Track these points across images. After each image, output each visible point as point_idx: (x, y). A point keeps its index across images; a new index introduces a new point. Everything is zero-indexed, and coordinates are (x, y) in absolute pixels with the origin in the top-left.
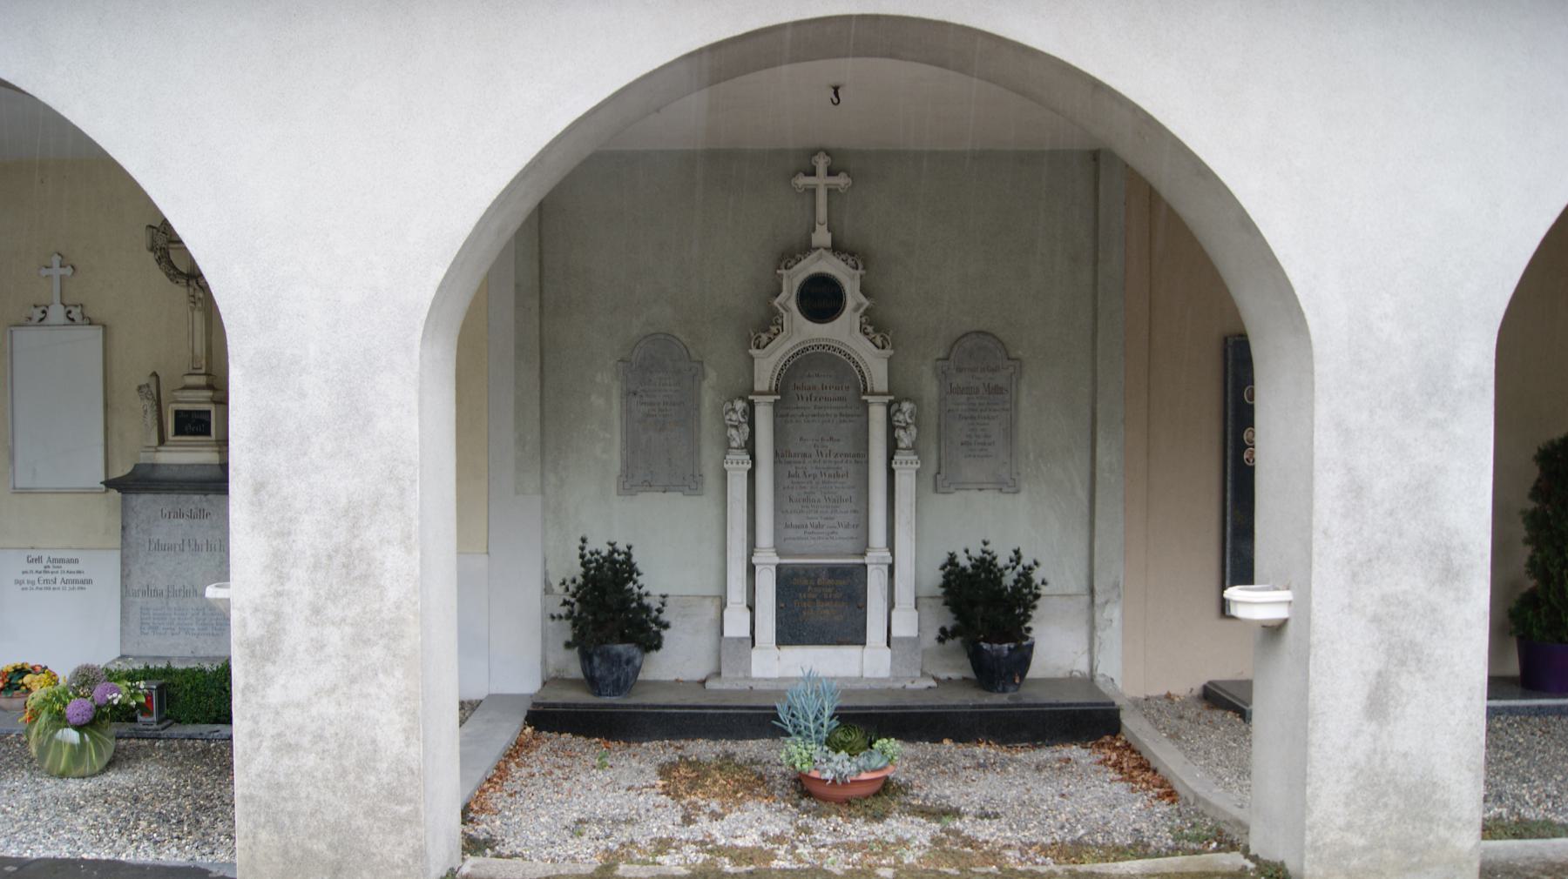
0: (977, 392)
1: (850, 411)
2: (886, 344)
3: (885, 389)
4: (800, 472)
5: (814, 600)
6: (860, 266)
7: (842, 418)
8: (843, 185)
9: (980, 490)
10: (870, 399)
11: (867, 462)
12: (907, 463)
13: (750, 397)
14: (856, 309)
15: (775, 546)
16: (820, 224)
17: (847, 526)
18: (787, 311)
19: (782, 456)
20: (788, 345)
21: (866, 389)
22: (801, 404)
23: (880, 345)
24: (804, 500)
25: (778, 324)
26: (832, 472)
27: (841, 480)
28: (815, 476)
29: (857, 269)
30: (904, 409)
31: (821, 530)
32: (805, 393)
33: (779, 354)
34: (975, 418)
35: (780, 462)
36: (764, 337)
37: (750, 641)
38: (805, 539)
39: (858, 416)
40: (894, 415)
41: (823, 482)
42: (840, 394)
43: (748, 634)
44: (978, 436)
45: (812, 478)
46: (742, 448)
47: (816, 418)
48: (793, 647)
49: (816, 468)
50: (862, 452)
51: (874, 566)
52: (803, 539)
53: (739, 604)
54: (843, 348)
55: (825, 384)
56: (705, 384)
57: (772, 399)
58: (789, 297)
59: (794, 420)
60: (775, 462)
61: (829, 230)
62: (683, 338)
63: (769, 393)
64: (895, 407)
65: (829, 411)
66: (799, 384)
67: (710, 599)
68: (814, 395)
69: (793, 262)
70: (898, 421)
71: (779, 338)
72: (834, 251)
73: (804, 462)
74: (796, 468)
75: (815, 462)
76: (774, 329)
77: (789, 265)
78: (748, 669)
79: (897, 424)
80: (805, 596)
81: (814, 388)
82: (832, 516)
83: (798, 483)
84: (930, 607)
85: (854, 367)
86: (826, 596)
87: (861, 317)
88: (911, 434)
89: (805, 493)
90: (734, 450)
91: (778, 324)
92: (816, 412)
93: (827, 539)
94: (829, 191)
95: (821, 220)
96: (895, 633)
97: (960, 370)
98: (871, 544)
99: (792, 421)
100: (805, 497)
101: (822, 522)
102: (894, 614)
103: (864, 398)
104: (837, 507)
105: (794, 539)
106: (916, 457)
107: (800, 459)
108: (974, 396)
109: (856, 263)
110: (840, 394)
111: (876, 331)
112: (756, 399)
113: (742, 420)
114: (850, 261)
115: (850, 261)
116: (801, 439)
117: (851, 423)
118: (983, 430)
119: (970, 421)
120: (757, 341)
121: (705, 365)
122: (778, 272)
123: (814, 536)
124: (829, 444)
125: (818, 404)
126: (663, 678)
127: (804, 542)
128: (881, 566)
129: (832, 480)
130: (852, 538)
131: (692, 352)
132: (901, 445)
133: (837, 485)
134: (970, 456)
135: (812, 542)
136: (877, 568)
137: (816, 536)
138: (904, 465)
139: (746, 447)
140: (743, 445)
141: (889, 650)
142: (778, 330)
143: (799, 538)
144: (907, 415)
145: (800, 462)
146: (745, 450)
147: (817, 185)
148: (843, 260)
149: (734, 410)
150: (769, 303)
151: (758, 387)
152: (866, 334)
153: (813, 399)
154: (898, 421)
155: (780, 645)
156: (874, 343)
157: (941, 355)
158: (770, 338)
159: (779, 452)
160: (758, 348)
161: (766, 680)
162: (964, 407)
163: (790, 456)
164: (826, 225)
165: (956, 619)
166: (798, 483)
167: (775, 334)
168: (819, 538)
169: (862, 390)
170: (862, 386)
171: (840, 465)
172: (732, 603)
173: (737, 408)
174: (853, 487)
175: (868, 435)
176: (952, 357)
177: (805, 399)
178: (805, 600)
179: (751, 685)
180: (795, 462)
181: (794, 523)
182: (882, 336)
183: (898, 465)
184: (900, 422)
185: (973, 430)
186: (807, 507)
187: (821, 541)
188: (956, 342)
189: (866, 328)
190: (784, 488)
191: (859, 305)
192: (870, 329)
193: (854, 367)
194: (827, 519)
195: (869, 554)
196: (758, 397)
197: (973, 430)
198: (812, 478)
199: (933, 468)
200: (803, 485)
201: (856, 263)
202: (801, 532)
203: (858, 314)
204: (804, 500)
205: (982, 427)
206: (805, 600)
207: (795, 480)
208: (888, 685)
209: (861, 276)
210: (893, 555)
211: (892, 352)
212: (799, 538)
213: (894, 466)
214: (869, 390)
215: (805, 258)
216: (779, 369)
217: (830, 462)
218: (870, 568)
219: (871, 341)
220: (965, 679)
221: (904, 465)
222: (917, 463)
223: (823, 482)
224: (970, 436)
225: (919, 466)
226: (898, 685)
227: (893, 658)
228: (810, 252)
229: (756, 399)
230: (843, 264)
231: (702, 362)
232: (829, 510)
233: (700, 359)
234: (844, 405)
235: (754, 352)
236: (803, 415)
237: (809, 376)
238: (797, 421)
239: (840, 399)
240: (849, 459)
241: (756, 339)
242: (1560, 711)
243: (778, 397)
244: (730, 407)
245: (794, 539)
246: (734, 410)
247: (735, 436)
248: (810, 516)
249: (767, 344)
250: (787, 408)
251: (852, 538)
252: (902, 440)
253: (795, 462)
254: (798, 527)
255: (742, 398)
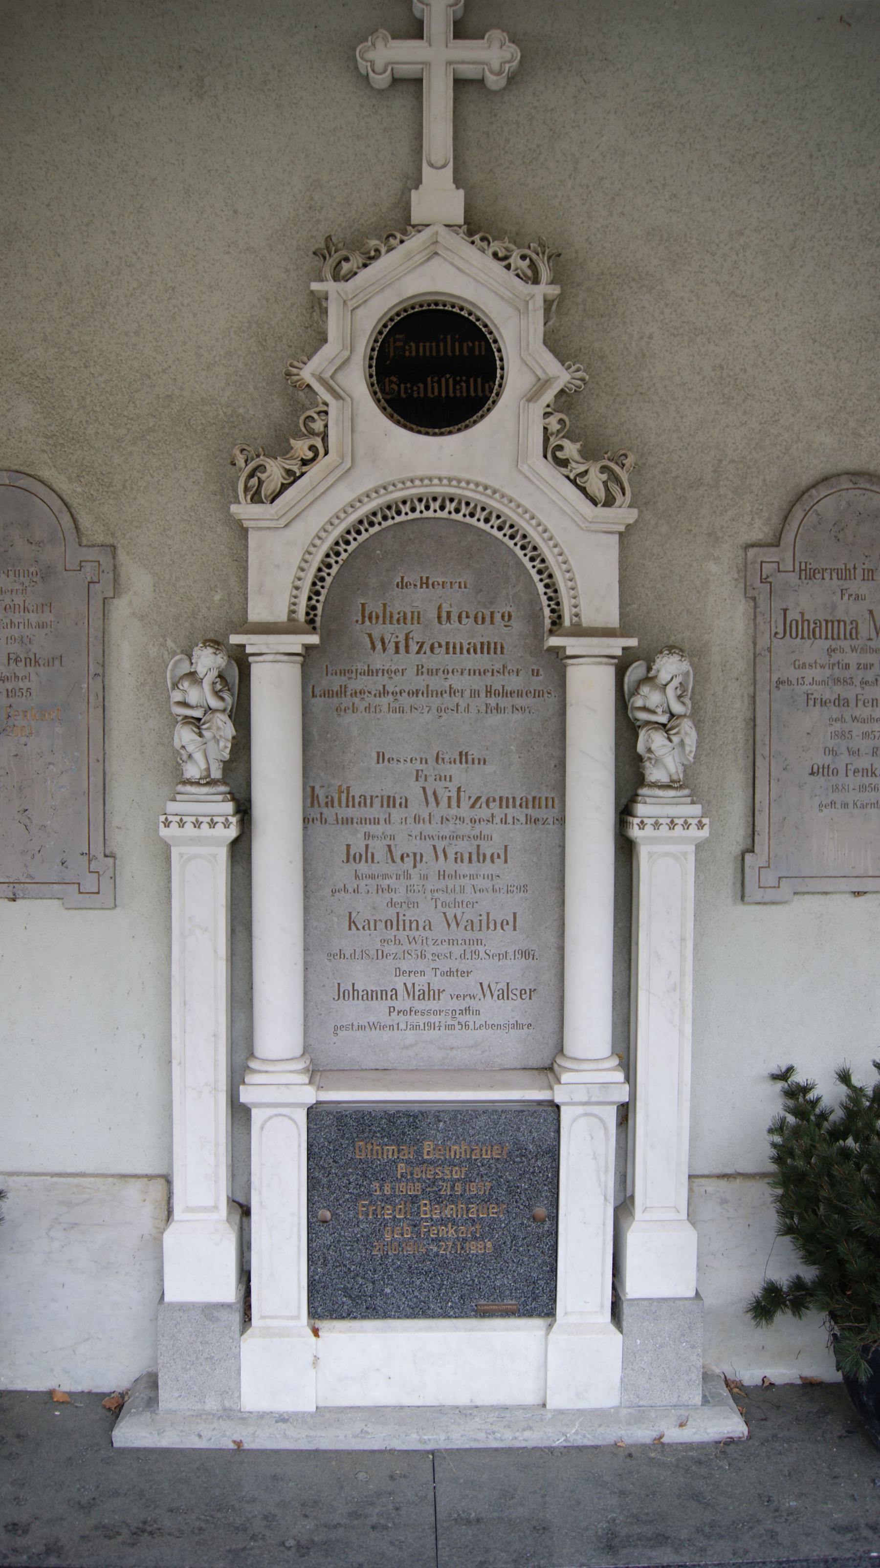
0: (853, 634)
1: (514, 682)
2: (615, 489)
3: (614, 621)
4: (378, 847)
5: (414, 1199)
6: (545, 274)
7: (492, 701)
8: (496, 66)
9: (857, 894)
10: (572, 645)
11: (562, 820)
12: (672, 825)
13: (235, 639)
14: (532, 397)
15: (307, 1049)
16: (431, 165)
17: (505, 994)
18: (337, 396)
19: (330, 804)
20: (343, 495)
21: (557, 621)
22: (378, 660)
23: (601, 495)
24: (389, 924)
25: (312, 433)
26: (464, 846)
27: (487, 868)
28: (417, 858)
29: (536, 281)
30: (664, 677)
31: (433, 1005)
32: (392, 632)
33: (315, 520)
34: (847, 702)
35: (323, 821)
36: (274, 472)
37: (236, 1317)
38: (391, 1027)
39: (538, 694)
40: (635, 691)
41: (442, 875)
42: (485, 633)
43: (229, 1293)
44: (854, 753)
45: (409, 861)
46: (212, 783)
47: (421, 700)
48: (356, 1324)
49: (422, 836)
50: (546, 793)
51: (580, 1110)
52: (383, 1027)
53: (205, 1209)
54: (494, 504)
55: (446, 608)
56: (121, 609)
57: (295, 643)
58: (347, 361)
59: (362, 705)
60: (306, 821)
61: (458, 182)
62: (61, 483)
63: (289, 628)
64: (635, 672)
65: (456, 681)
66: (374, 607)
67: (139, 1184)
68: (417, 636)
69: (356, 260)
70: (645, 709)
71: (315, 471)
72: (470, 233)
73: (388, 821)
74: (367, 836)
75: (417, 819)
76: (301, 448)
77: (346, 266)
78: (233, 1389)
79: (643, 716)
80: (387, 1190)
81: (418, 617)
82: (463, 966)
83: (372, 877)
84: (723, 1201)
85: (526, 560)
86: (446, 1191)
87: (547, 415)
88: (682, 743)
89: (392, 903)
90: (189, 788)
91: (312, 433)
92: (421, 682)
93: (451, 1027)
94: (460, 83)
95: (438, 159)
96: (633, 1289)
97: (809, 574)
98: (569, 1049)
99: (354, 710)
100: (391, 913)
101: (437, 983)
102: (633, 1239)
103: (554, 641)
104: (479, 942)
105: (361, 1028)
106: (697, 809)
107: (375, 811)
108: (846, 644)
109: (533, 266)
110: (485, 633)
111: (588, 454)
112: (253, 643)
113: (214, 703)
114: (515, 260)
115: (515, 260)
116: (381, 757)
117: (518, 716)
118: (866, 735)
119: (835, 712)
120: (254, 481)
121: (122, 556)
122: (315, 286)
123: (413, 1019)
124: (455, 770)
125: (423, 659)
126: (19, 1385)
127: (386, 1035)
128: (596, 1110)
129: (464, 868)
130: (517, 1026)
131: (85, 521)
132: (654, 774)
133: (480, 883)
134: (833, 804)
135: (411, 1036)
136: (586, 1114)
137: (420, 1020)
138: (664, 830)
139: (223, 781)
140: (216, 774)
141: (621, 1335)
142: (312, 448)
143: (373, 1026)
144: (670, 691)
145: (377, 821)
146: (223, 788)
147: (427, 64)
148: (495, 255)
149: (192, 676)
150: (289, 374)
151: (257, 613)
152: (563, 463)
153: (414, 648)
154: (645, 709)
155: (320, 1317)
156: (583, 490)
157: (759, 531)
158: (289, 472)
159: (321, 793)
160: (256, 498)
161: (282, 1418)
162: (818, 674)
163: (350, 802)
164: (450, 169)
165: (813, 1282)
166: (372, 877)
167: (305, 462)
168: (431, 1026)
169: (547, 622)
170: (547, 612)
171: (487, 829)
172: (189, 1209)
173: (201, 670)
174: (524, 888)
175: (563, 749)
176: (788, 538)
177: (391, 647)
178: (387, 1200)
179: (237, 1438)
180: (364, 821)
181: (359, 987)
182: (604, 469)
183: (649, 831)
184: (653, 712)
185: (841, 735)
186: (397, 941)
187: (435, 1033)
188: (799, 498)
189: (560, 448)
190: (333, 892)
191: (542, 385)
192: (571, 450)
193: (526, 560)
194: (450, 973)
195: (565, 1077)
196: (254, 638)
197: (841, 735)
198: (409, 861)
199: (736, 837)
200: (385, 883)
201: (533, 266)
202: (379, 1010)
203: (538, 408)
204: (389, 924)
205: (866, 728)
206: (387, 1200)
207: (363, 868)
208: (606, 1435)
209: (548, 304)
210: (630, 1077)
211: (632, 515)
212: (373, 1026)
213: (635, 832)
214: (567, 622)
215: (390, 249)
216: (316, 563)
217: (462, 820)
218: (566, 1114)
219: (574, 482)
220: (809, 1386)
221: (664, 830)
222: (700, 826)
223: (442, 875)
224: (833, 752)
225: (705, 833)
226: (643, 1434)
227: (629, 1357)
228: (404, 232)
229: (253, 643)
230: (497, 267)
231: (113, 547)
232: (457, 950)
233: (110, 540)
234: (498, 666)
235: (244, 510)
236: (384, 692)
237: (402, 585)
238: (367, 709)
239: (486, 648)
240: (511, 812)
241: (251, 475)
242: (875, 805)
243: (314, 639)
244: (185, 668)
245: (361, 1028)
246: (192, 676)
247: (190, 748)
248: (405, 966)
249: (284, 487)
250: (343, 673)
251: (517, 1026)
252: (658, 761)
253: (364, 821)
254: (371, 995)
255: (216, 644)
